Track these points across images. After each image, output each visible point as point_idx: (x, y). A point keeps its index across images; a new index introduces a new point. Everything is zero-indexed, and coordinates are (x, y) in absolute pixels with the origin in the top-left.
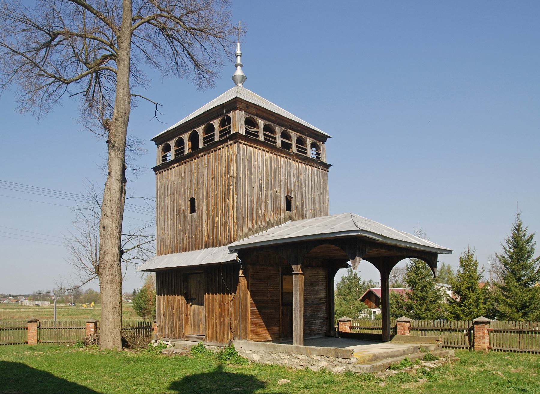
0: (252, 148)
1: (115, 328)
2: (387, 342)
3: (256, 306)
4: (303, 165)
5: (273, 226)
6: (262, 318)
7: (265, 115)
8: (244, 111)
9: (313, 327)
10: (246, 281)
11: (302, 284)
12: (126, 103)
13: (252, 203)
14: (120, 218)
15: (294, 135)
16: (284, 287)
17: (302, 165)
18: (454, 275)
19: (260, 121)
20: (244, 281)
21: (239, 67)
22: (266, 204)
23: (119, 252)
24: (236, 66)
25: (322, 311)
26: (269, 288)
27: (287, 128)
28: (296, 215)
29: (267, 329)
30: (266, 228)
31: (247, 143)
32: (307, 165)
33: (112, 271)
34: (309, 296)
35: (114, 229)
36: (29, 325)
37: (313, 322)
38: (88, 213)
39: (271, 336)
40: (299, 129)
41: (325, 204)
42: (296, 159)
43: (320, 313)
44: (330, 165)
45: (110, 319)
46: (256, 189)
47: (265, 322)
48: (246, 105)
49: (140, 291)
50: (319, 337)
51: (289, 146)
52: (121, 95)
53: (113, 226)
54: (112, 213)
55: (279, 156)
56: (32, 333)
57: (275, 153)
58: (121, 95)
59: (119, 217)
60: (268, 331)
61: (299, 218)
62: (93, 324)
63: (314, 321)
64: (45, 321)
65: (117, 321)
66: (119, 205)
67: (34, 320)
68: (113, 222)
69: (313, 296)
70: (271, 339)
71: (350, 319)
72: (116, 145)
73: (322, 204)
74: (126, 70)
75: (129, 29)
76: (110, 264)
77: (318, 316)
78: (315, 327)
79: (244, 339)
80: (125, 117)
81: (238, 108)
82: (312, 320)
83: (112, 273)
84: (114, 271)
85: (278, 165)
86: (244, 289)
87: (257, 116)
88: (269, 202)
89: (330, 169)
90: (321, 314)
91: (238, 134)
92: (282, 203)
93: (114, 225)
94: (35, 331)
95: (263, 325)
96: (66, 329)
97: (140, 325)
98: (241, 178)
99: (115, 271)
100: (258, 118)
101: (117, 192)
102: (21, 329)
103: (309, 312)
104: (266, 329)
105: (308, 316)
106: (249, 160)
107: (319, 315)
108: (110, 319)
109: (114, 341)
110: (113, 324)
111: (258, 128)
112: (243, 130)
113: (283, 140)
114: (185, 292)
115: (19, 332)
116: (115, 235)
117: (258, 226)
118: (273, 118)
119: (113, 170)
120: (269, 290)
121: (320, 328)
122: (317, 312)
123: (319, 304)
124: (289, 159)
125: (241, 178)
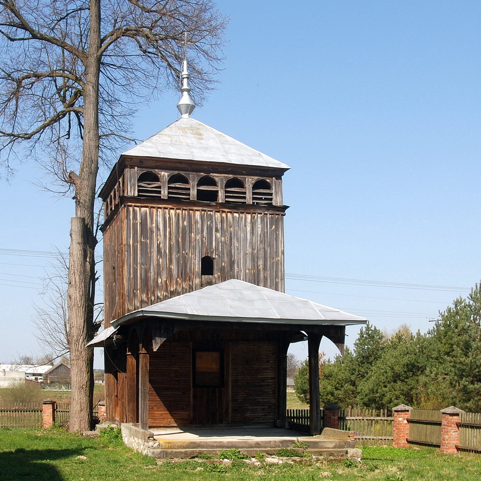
0: (147, 209)
1: (81, 410)
2: (313, 436)
3: (153, 387)
4: (236, 215)
6: (161, 401)
7: (169, 164)
8: (138, 167)
9: (248, 415)
10: (134, 359)
11: (146, 364)
12: (93, 148)
14: (85, 286)
15: (222, 180)
16: (197, 365)
19: (163, 173)
20: (131, 359)
21: (185, 93)
23: (85, 324)
24: (182, 91)
25: (266, 395)
26: (173, 367)
27: (208, 173)
29: (170, 413)
30: (166, 298)
31: (140, 205)
32: (242, 213)
33: (78, 347)
34: (241, 377)
35: (78, 299)
36: (45, 407)
37: (249, 408)
38: (58, 281)
39: (176, 422)
40: (229, 169)
42: (221, 209)
43: (261, 398)
44: (286, 207)
45: (76, 400)
47: (165, 405)
48: (139, 160)
49: (304, 364)
50: (262, 427)
51: (214, 195)
52: (87, 139)
53: (76, 295)
54: (75, 281)
56: (47, 416)
57: (185, 208)
58: (87, 139)
59: (83, 285)
60: (171, 415)
61: (219, 282)
62: (51, 405)
63: (251, 408)
64: (232, 407)
65: (83, 403)
66: (82, 271)
67: (49, 401)
68: (77, 291)
69: (248, 376)
70: (176, 425)
72: (81, 201)
74: (92, 108)
75: (95, 55)
76: (75, 338)
77: (259, 402)
78: (252, 414)
79: (131, 422)
80: (91, 166)
81: (129, 166)
82: (247, 405)
83: (78, 349)
84: (80, 347)
86: (131, 368)
87: (158, 168)
89: (287, 211)
90: (263, 399)
91: (123, 197)
92: (197, 266)
93: (78, 295)
94: (50, 414)
95: (163, 408)
96: (66, 412)
97: (303, 413)
98: (132, 246)
99: (81, 346)
100: (160, 170)
101: (78, 257)
102: (38, 411)
103: (242, 396)
104: (169, 413)
105: (239, 400)
106: (144, 223)
107: (260, 400)
108: (76, 400)
109: (81, 425)
110: (79, 406)
114: (114, 371)
115: (35, 414)
116: (79, 306)
118: (183, 166)
119: (73, 233)
120: (172, 369)
121: (262, 416)
122: (257, 396)
123: (261, 386)
125: (132, 246)
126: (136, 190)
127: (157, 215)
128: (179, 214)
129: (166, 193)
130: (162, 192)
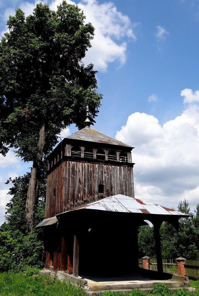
5: (88, 202)
13: (74, 190)
14: (35, 199)
17: (111, 166)
18: (7, 223)
22: (84, 190)
28: (107, 194)
41: (130, 186)
46: (77, 183)
54: (31, 197)
55: (95, 164)
59: (34, 198)
71: (184, 259)
73: (127, 187)
85: (93, 169)
88: (86, 189)
92: (96, 188)
111: (81, 151)
112: (70, 154)
113: (98, 154)
117: (78, 203)
124: (102, 164)
126: (70, 154)
127: (79, 165)
128: (88, 165)
129: (83, 155)
130: (81, 155)
